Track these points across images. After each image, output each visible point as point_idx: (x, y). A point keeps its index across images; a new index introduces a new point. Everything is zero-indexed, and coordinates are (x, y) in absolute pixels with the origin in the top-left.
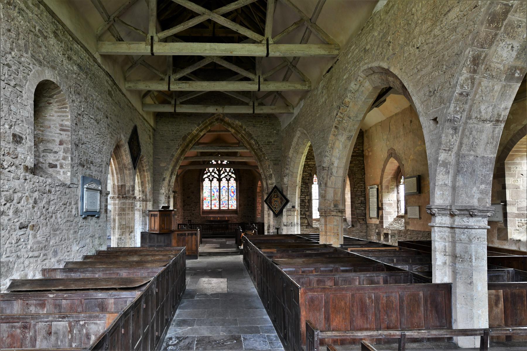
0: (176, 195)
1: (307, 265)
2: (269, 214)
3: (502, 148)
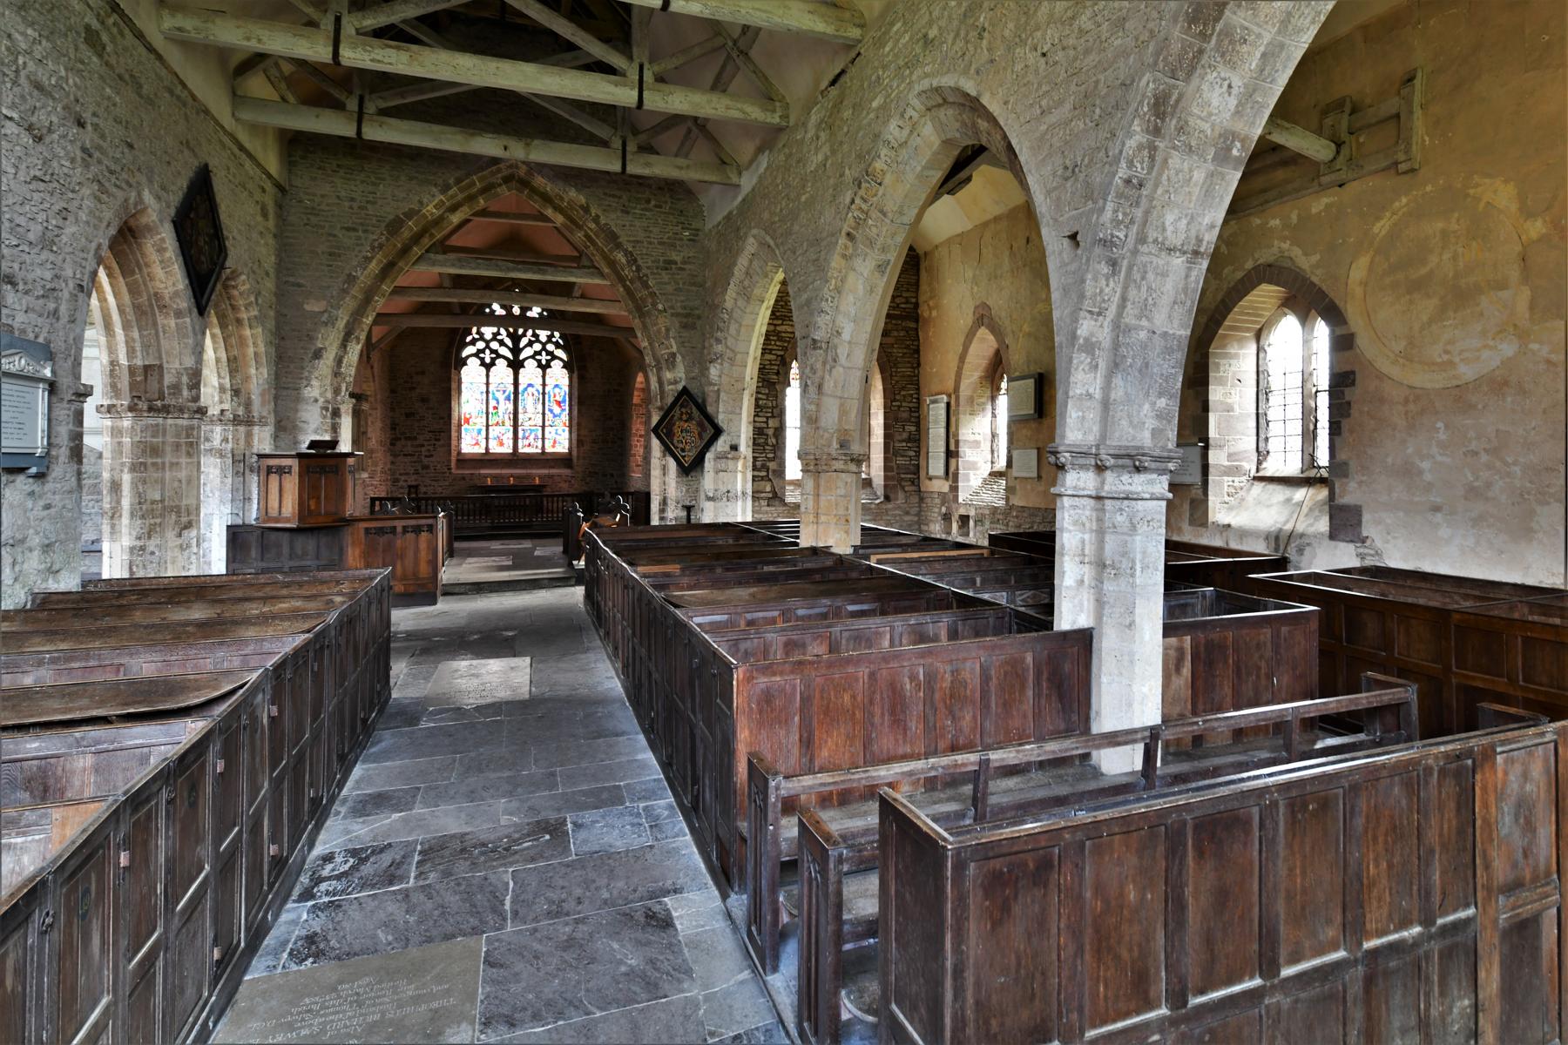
0: (365, 406)
1: (761, 603)
2: (664, 469)
3: (1204, 320)
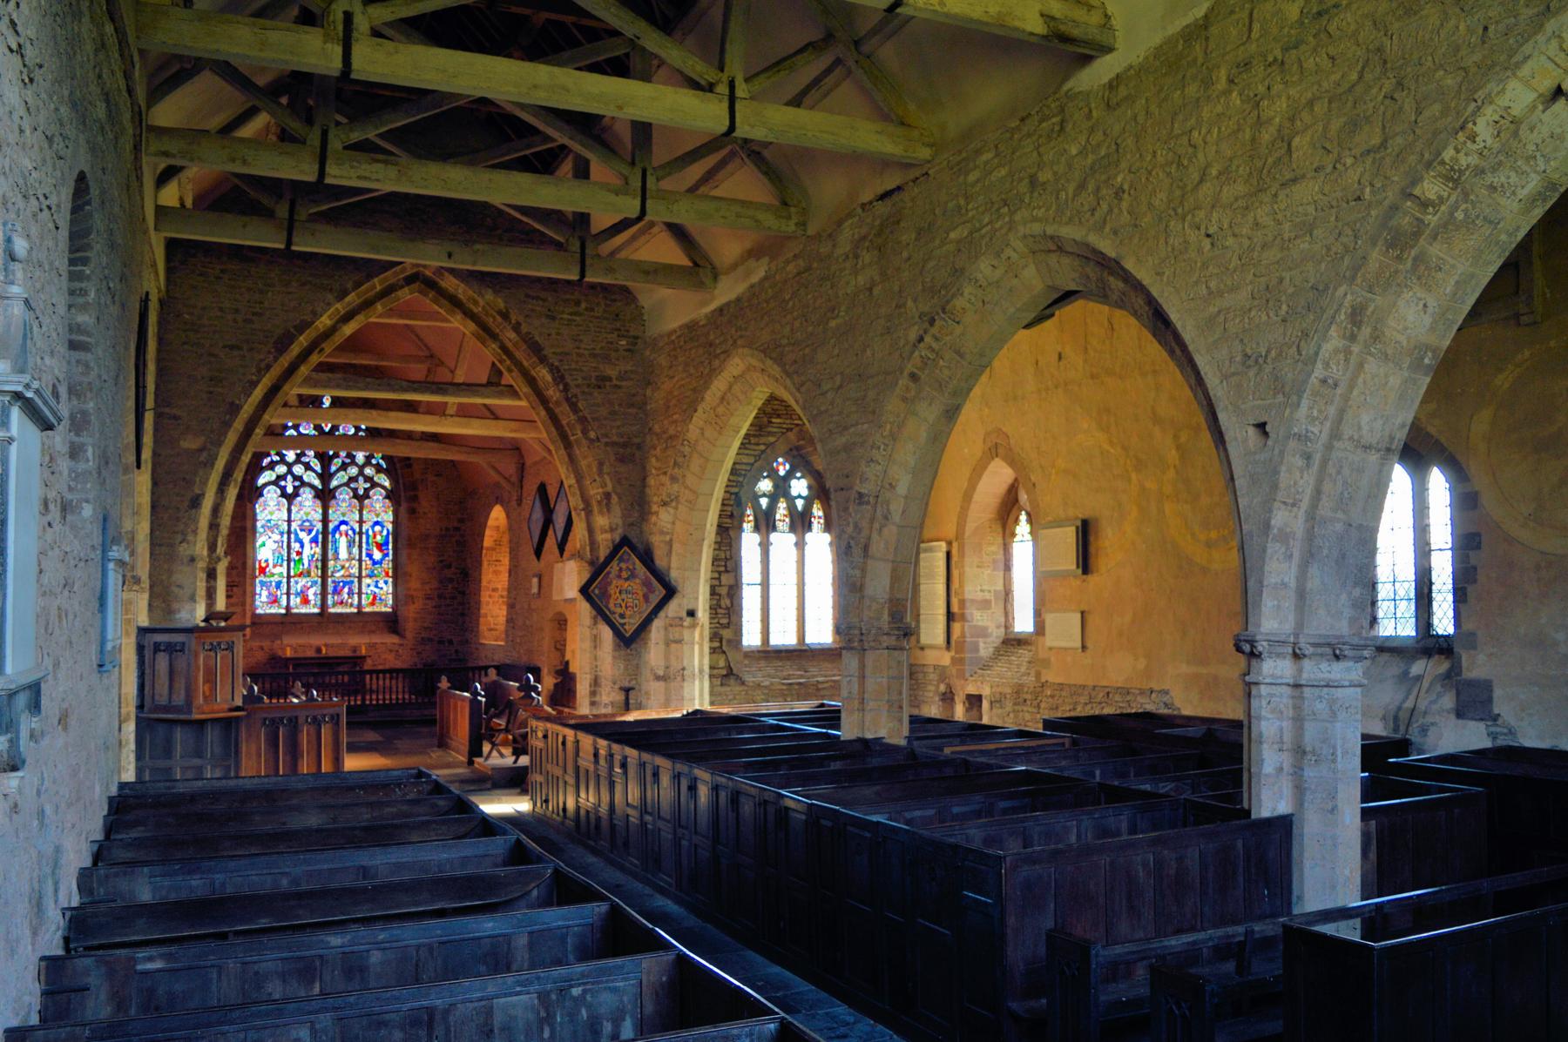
2: (596, 641)
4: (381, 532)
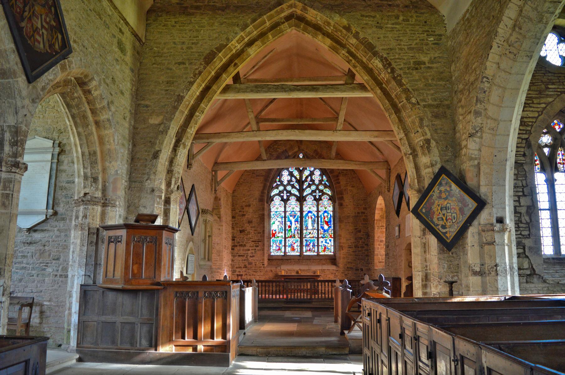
2: (425, 247)
4: (327, 216)
